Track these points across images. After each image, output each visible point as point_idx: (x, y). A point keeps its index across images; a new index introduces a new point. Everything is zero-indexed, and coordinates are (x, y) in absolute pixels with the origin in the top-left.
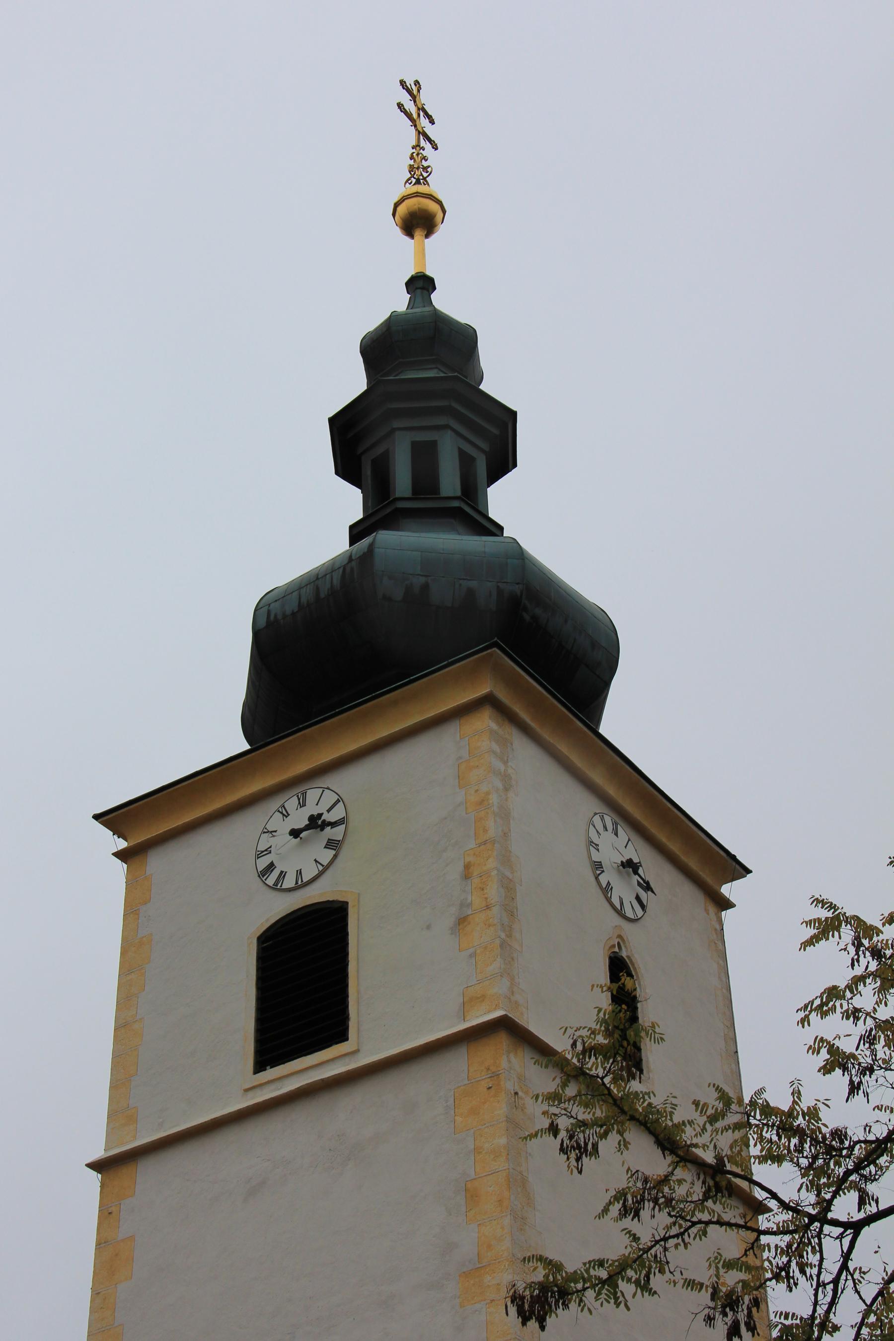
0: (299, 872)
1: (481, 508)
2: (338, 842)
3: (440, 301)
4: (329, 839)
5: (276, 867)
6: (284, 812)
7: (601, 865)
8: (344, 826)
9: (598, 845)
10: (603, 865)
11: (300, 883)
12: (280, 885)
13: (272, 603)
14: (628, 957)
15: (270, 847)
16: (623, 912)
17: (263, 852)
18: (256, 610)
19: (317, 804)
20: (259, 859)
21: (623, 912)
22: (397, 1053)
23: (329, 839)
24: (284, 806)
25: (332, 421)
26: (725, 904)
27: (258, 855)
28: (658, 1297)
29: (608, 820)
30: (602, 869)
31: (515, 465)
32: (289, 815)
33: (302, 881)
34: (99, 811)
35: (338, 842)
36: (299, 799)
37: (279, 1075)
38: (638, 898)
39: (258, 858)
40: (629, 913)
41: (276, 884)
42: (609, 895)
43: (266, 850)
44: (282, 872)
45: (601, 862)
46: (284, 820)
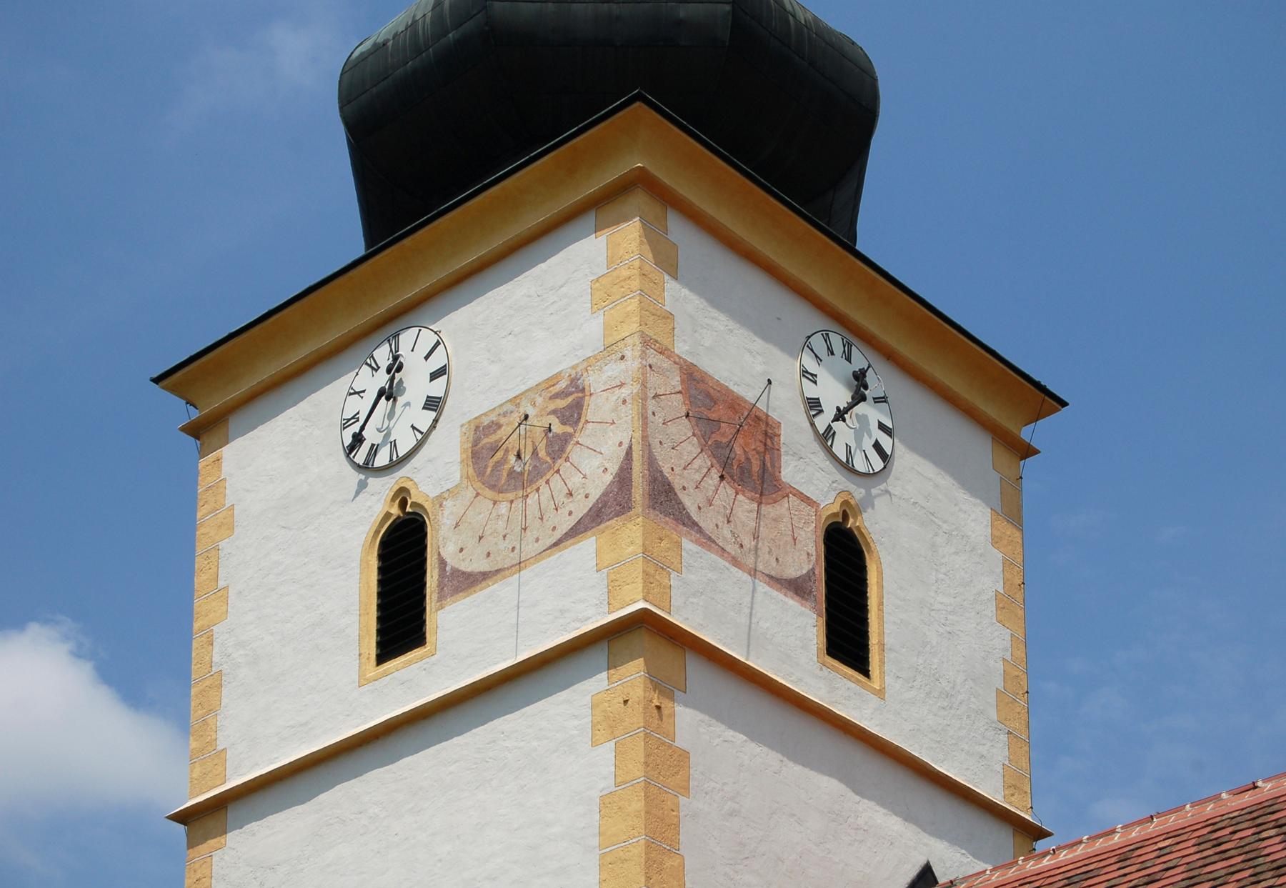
0: (393, 443)
2: (438, 400)
4: (428, 397)
6: (374, 365)
7: (819, 402)
8: (445, 377)
9: (816, 376)
12: (371, 463)
13: (369, 56)
14: (858, 528)
15: (358, 413)
16: (851, 466)
17: (349, 420)
18: (341, 74)
19: (412, 350)
20: (345, 430)
21: (851, 466)
23: (428, 397)
24: (372, 357)
26: (1027, 451)
27: (344, 424)
29: (836, 341)
30: (820, 408)
32: (379, 368)
33: (398, 456)
34: (155, 375)
35: (438, 400)
37: (1111, 866)
38: (877, 446)
39: (344, 428)
40: (860, 465)
41: (366, 463)
42: (829, 444)
43: (353, 418)
44: (373, 445)
45: (818, 399)
46: (373, 376)
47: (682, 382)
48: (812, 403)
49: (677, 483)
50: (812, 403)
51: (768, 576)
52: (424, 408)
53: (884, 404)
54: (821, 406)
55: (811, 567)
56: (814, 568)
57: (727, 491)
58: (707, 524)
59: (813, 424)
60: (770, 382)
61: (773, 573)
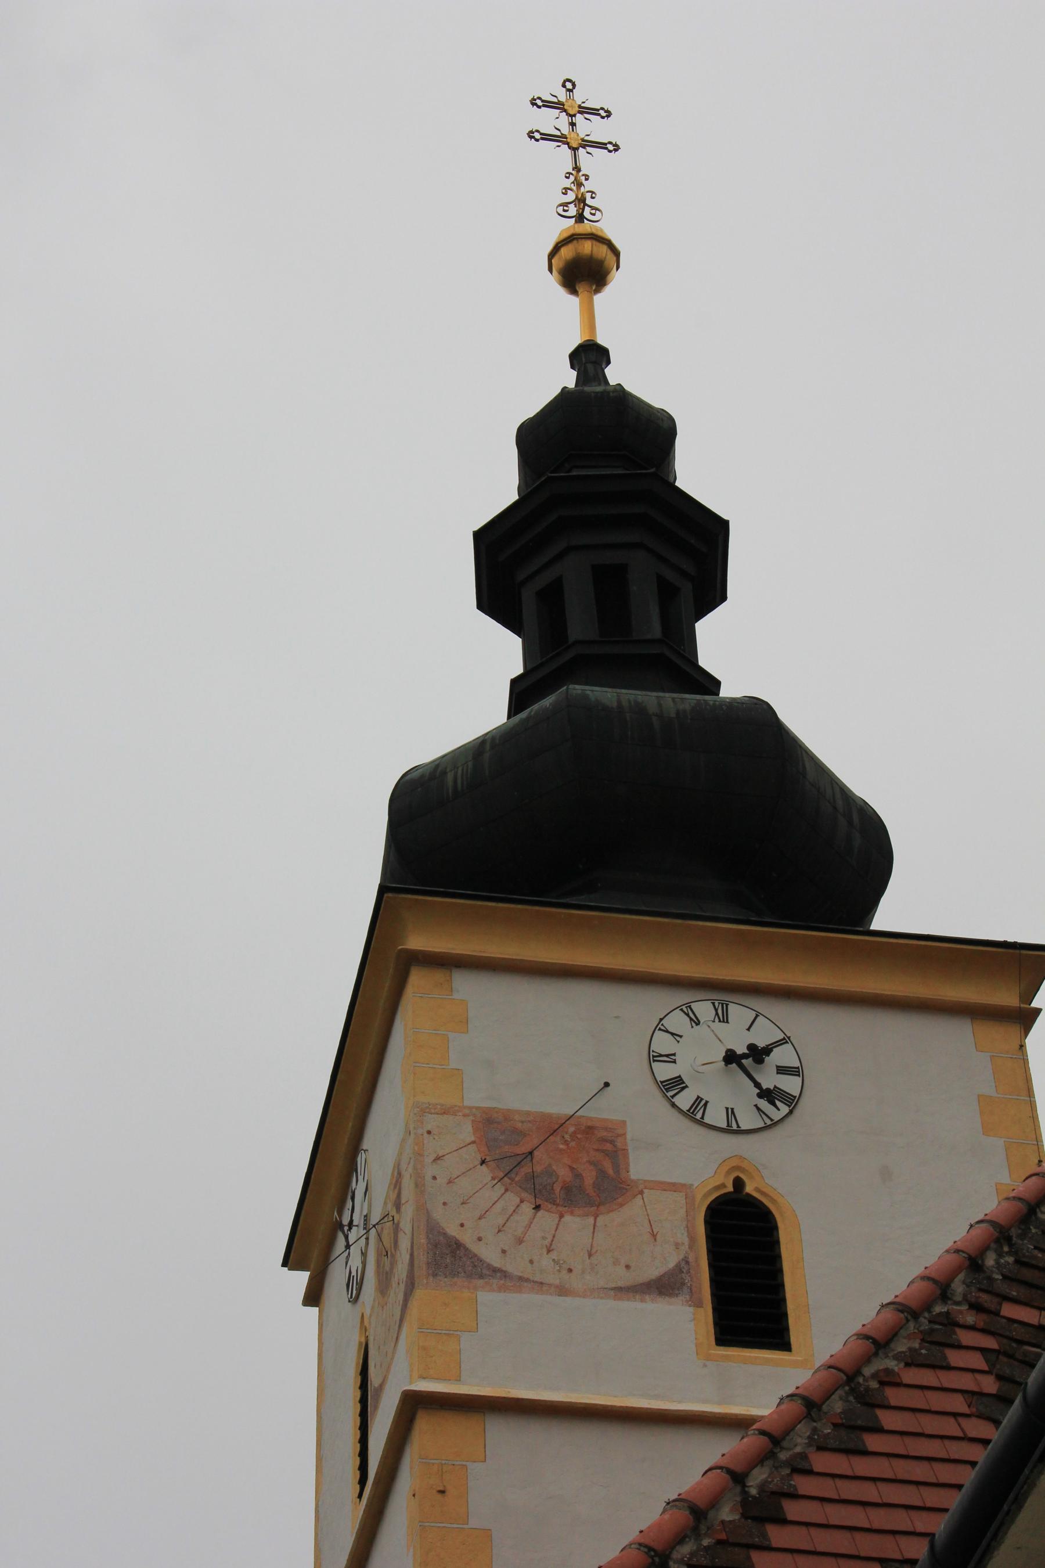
2: (725, 1005)
3: (614, 375)
7: (682, 1079)
9: (674, 1055)
10: (684, 1080)
17: (661, 1056)
25: (479, 536)
28: (403, 1234)
31: (724, 598)
35: (725, 1005)
36: (716, 1010)
44: (699, 1099)
45: (680, 1076)
47: (476, 1130)
48: (667, 1085)
49: (467, 1238)
50: (667, 1085)
51: (612, 1289)
52: (727, 1022)
53: (786, 1045)
54: (684, 1083)
55: (681, 1257)
56: (685, 1257)
57: (546, 1219)
58: (515, 1266)
59: (673, 1105)
60: (607, 1085)
61: (620, 1284)
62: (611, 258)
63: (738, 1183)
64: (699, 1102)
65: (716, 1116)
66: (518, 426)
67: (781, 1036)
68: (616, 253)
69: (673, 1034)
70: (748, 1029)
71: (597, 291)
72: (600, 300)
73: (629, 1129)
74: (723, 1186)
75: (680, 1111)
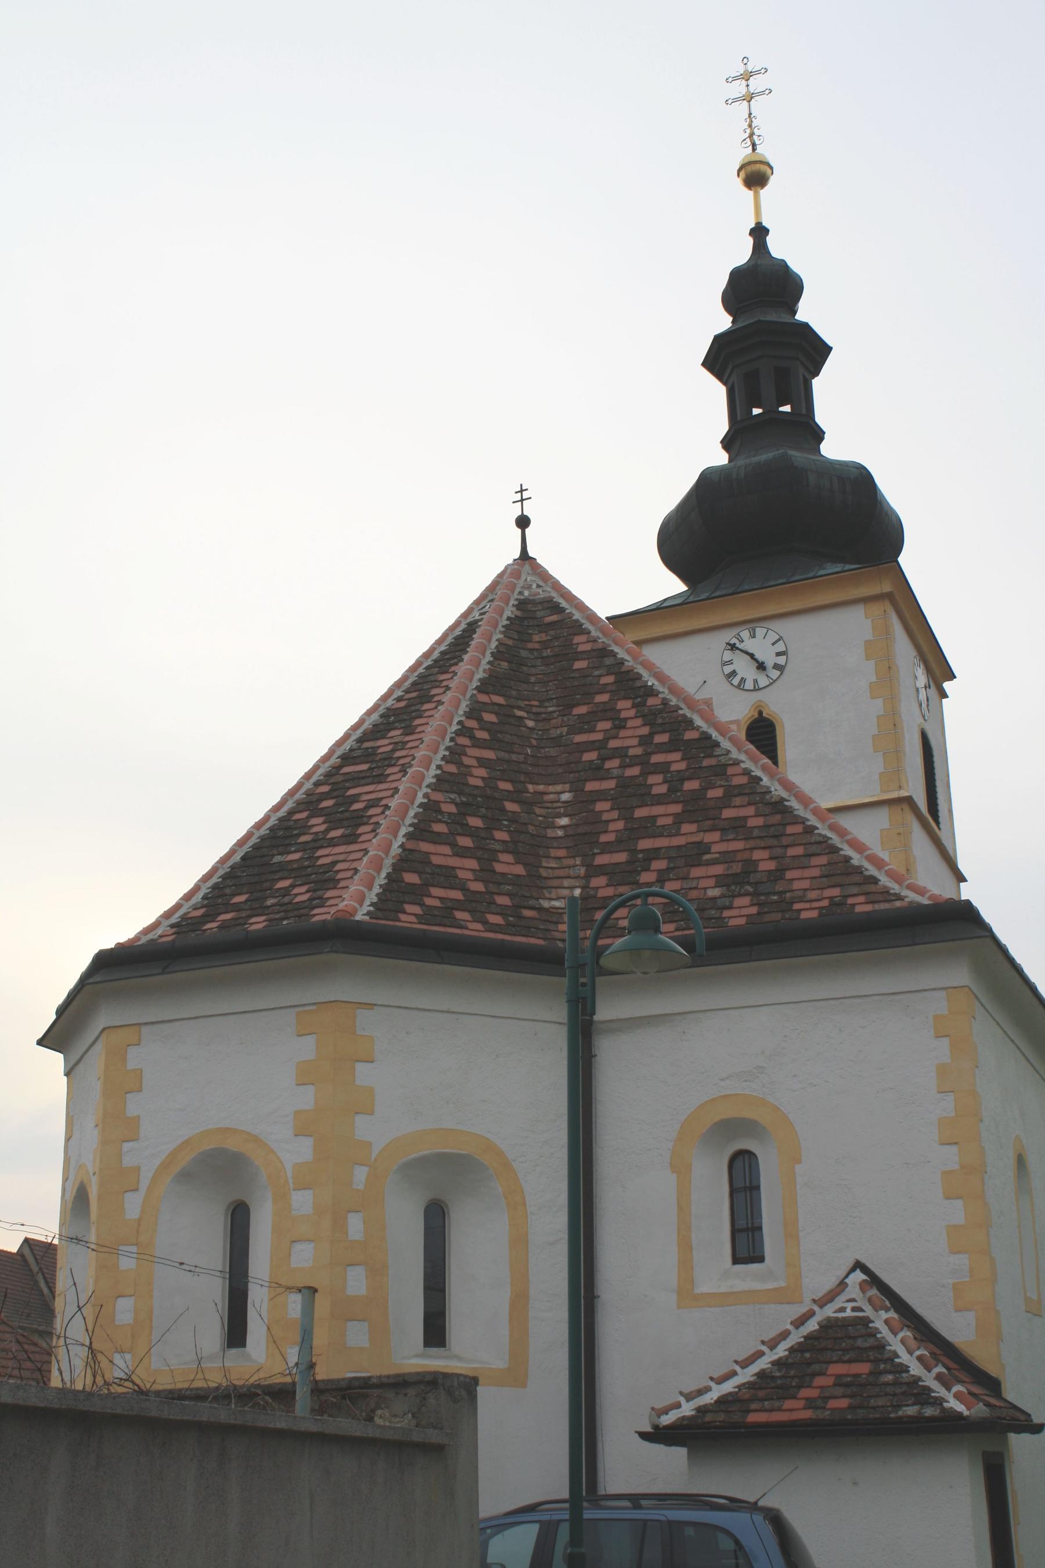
1: (943, 835)
5: (745, 679)
11: (757, 687)
17: (726, 662)
22: (325, 754)
36: (750, 632)
44: (742, 678)
59: (732, 684)
60: (705, 682)
62: (769, 171)
63: (760, 713)
64: (743, 680)
65: (749, 685)
66: (722, 291)
67: (778, 637)
68: (771, 168)
69: (261, 1316)
70: (764, 638)
71: (762, 189)
72: (764, 192)
73: (714, 700)
74: (753, 716)
75: (734, 686)
